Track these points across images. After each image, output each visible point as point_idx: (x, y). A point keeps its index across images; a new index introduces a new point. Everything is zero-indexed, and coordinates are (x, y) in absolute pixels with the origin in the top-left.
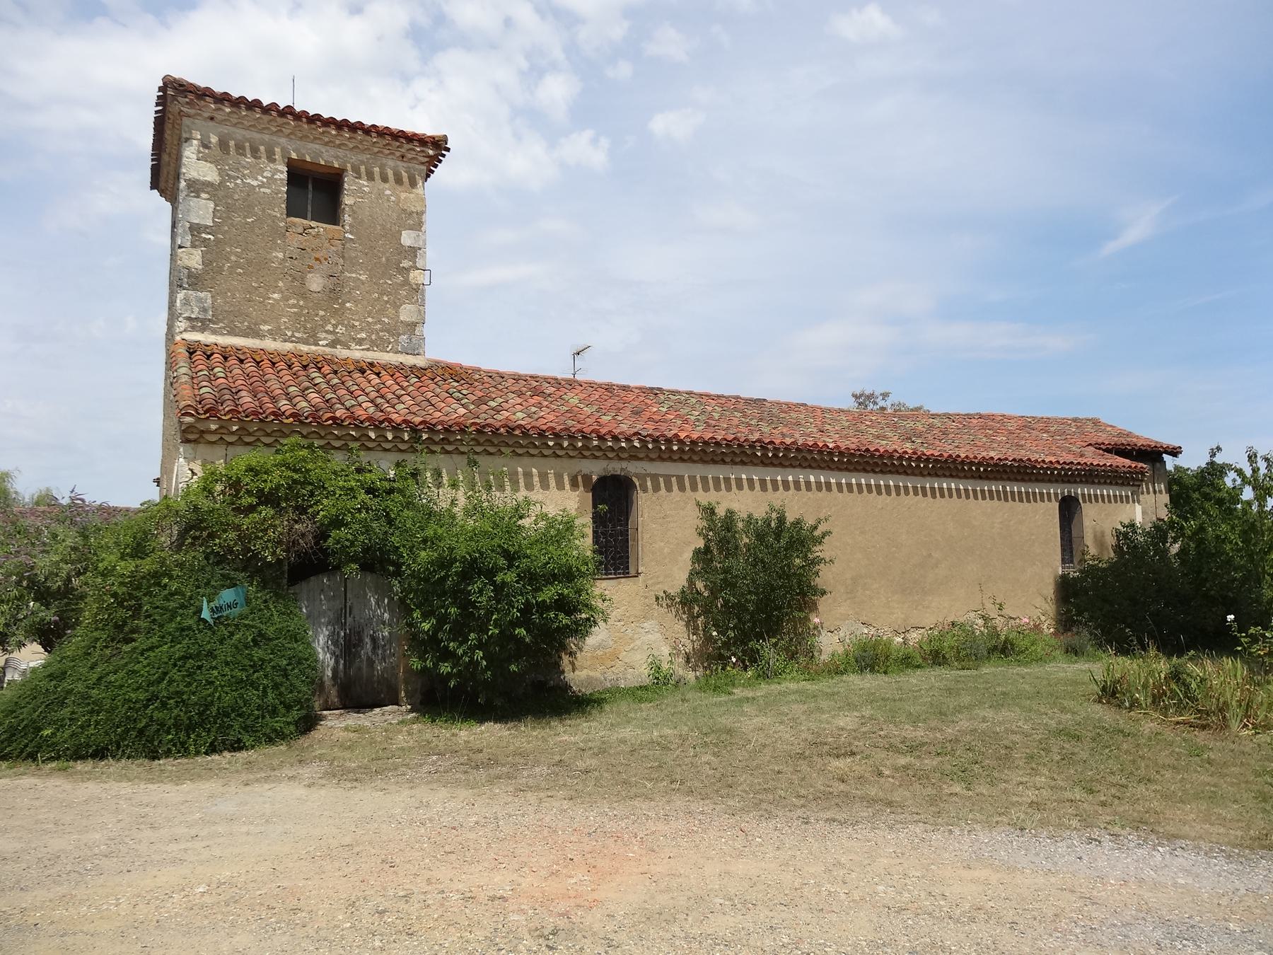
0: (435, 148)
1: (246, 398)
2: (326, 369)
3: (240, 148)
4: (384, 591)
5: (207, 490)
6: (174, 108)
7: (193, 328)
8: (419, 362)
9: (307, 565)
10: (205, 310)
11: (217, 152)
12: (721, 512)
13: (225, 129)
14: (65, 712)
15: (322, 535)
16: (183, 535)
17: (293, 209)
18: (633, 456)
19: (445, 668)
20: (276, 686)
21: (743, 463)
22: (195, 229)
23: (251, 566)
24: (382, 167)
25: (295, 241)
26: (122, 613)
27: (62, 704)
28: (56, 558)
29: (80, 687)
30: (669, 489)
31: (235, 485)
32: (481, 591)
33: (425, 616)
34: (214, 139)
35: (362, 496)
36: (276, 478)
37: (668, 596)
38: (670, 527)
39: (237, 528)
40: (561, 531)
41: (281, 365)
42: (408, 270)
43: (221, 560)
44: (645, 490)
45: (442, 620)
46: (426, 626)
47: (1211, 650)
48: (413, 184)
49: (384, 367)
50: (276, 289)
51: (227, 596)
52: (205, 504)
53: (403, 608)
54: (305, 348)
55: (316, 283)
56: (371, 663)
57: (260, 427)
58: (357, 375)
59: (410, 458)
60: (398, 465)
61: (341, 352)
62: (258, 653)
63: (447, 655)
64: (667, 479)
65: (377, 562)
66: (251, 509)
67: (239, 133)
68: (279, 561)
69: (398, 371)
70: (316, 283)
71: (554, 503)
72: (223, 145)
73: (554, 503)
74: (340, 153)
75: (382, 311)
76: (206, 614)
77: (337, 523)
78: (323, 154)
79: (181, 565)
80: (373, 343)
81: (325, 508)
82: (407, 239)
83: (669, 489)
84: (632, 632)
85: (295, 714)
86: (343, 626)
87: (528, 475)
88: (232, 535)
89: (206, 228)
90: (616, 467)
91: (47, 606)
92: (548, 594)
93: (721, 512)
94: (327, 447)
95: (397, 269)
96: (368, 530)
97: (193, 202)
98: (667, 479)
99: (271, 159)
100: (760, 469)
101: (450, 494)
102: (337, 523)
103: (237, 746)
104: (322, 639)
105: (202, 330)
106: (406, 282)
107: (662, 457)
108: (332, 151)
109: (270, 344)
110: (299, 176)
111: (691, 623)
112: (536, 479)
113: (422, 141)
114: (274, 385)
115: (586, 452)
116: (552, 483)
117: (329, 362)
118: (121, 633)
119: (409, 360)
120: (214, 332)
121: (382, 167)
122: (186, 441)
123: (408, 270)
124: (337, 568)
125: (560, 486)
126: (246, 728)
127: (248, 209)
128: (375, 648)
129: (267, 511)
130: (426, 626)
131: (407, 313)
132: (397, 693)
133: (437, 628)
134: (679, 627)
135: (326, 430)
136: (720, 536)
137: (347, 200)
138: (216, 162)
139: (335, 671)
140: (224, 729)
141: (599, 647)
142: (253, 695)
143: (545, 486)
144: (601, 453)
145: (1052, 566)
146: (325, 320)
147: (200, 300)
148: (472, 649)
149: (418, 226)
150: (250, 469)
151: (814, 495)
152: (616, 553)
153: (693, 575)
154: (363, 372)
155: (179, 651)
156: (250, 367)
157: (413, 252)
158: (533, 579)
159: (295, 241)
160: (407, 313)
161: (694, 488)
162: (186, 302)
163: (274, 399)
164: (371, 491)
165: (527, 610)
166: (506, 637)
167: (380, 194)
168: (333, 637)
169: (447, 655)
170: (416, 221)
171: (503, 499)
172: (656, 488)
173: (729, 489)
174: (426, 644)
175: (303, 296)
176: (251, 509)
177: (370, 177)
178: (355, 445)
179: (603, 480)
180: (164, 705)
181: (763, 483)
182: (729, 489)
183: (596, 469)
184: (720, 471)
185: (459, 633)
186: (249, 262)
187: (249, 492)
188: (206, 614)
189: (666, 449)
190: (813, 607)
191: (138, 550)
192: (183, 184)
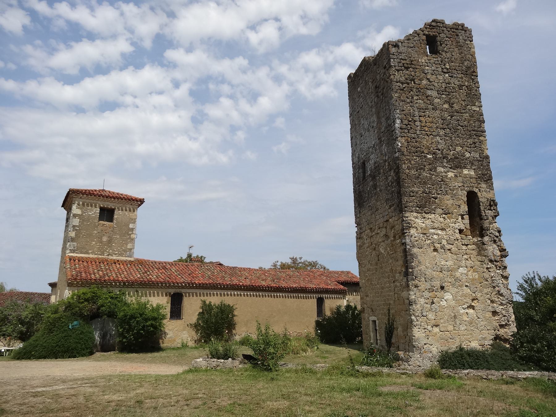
0: (142, 201)
1: (83, 274)
2: (105, 263)
3: (88, 205)
4: (113, 322)
5: (72, 298)
6: (71, 196)
7: (71, 252)
8: (132, 259)
9: (94, 316)
10: (74, 247)
11: (81, 206)
12: (207, 302)
13: (84, 200)
14: (37, 349)
15: (98, 309)
16: (66, 308)
17: (101, 218)
18: (183, 287)
19: (124, 340)
20: (85, 344)
21: (215, 289)
22: (74, 226)
23: (81, 316)
24: (126, 207)
25: (100, 228)
26: (51, 326)
27: (37, 347)
28: (27, 313)
29: (41, 343)
30: (193, 296)
31: (79, 297)
32: (133, 322)
33: (121, 328)
34: (81, 203)
35: (110, 299)
36: (89, 295)
37: (191, 325)
38: (192, 306)
39: (79, 307)
40: (159, 307)
41: (94, 263)
42: (130, 234)
43: (74, 314)
44: (186, 296)
45: (124, 329)
46: (121, 330)
47: (467, 350)
48: (134, 211)
49: (121, 262)
50: (94, 241)
51: (75, 323)
52: (71, 301)
53: (116, 327)
54: (100, 256)
55: (105, 239)
56: (109, 340)
57: (86, 283)
58: (114, 265)
59: (123, 289)
60: (120, 291)
61: (110, 257)
62: (81, 336)
63: (125, 337)
64: (189, 293)
65: (112, 315)
66: (83, 302)
67: (88, 201)
68: (88, 315)
69: (124, 263)
70: (105, 239)
71: (160, 301)
72: (83, 204)
73: (160, 301)
74: (114, 204)
75: (122, 246)
76: (70, 327)
77: (102, 306)
78: (109, 205)
79: (65, 316)
80: (119, 255)
81: (100, 302)
82: (131, 226)
83: (193, 296)
84: (178, 332)
85: (89, 350)
86: (103, 331)
87: (154, 293)
88: (78, 309)
89: (77, 226)
90: (178, 291)
91: (23, 326)
92: (149, 323)
93: (207, 302)
94: (102, 287)
95: (127, 234)
96: (110, 307)
97: (74, 220)
98: (189, 293)
99: (96, 207)
100: (220, 291)
101: (131, 299)
102: (102, 306)
103: (75, 357)
104: (97, 334)
105: (73, 253)
106: (130, 238)
107: (193, 288)
108: (112, 204)
109: (91, 256)
110: (103, 210)
111: (197, 332)
112: (156, 294)
113: (136, 200)
114: (91, 269)
115: (170, 287)
116: (160, 295)
117: (107, 260)
118: (51, 331)
119: (129, 259)
120: (77, 253)
121: (126, 207)
122: (68, 286)
123: (130, 234)
124: (102, 317)
125: (162, 296)
126: (77, 353)
127: (88, 221)
128: (110, 337)
129: (86, 303)
130: (121, 330)
131: (129, 246)
132: (115, 348)
133: (123, 331)
134: (194, 333)
135: (101, 283)
136: (207, 309)
137: (115, 217)
138: (81, 209)
139: (100, 342)
140: (72, 353)
141: (170, 338)
142: (79, 345)
143: (154, 296)
144: (174, 287)
145: (314, 317)
146: (107, 249)
147: (73, 245)
148: (131, 336)
149: (134, 222)
150: (83, 293)
151: (236, 297)
152: (176, 313)
153: (198, 319)
154: (115, 263)
155: (63, 335)
156: (85, 263)
157: (132, 229)
158: (146, 320)
159: (100, 228)
160: (129, 246)
161: (200, 296)
162: (70, 245)
163: (90, 274)
164: (112, 298)
165: (144, 326)
166: (138, 333)
167: (125, 214)
168: (100, 334)
169: (125, 337)
170: (134, 221)
171: (143, 300)
172: (189, 296)
173: (210, 296)
174: (121, 335)
175: (101, 243)
176: (83, 302)
177: (122, 210)
178: (109, 286)
179: (174, 294)
180: (60, 347)
181: (221, 294)
182: (210, 296)
183: (172, 291)
184: (208, 291)
185: (128, 332)
186: (88, 234)
187: (82, 299)
188: (70, 327)
189: (192, 286)
190: (234, 329)
191: (56, 312)
192: (72, 215)
